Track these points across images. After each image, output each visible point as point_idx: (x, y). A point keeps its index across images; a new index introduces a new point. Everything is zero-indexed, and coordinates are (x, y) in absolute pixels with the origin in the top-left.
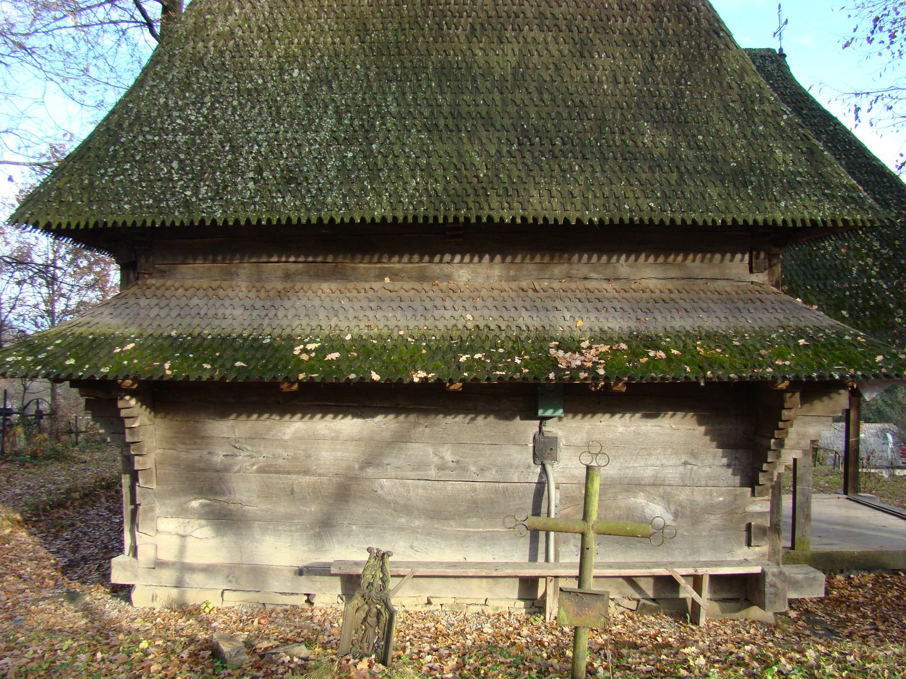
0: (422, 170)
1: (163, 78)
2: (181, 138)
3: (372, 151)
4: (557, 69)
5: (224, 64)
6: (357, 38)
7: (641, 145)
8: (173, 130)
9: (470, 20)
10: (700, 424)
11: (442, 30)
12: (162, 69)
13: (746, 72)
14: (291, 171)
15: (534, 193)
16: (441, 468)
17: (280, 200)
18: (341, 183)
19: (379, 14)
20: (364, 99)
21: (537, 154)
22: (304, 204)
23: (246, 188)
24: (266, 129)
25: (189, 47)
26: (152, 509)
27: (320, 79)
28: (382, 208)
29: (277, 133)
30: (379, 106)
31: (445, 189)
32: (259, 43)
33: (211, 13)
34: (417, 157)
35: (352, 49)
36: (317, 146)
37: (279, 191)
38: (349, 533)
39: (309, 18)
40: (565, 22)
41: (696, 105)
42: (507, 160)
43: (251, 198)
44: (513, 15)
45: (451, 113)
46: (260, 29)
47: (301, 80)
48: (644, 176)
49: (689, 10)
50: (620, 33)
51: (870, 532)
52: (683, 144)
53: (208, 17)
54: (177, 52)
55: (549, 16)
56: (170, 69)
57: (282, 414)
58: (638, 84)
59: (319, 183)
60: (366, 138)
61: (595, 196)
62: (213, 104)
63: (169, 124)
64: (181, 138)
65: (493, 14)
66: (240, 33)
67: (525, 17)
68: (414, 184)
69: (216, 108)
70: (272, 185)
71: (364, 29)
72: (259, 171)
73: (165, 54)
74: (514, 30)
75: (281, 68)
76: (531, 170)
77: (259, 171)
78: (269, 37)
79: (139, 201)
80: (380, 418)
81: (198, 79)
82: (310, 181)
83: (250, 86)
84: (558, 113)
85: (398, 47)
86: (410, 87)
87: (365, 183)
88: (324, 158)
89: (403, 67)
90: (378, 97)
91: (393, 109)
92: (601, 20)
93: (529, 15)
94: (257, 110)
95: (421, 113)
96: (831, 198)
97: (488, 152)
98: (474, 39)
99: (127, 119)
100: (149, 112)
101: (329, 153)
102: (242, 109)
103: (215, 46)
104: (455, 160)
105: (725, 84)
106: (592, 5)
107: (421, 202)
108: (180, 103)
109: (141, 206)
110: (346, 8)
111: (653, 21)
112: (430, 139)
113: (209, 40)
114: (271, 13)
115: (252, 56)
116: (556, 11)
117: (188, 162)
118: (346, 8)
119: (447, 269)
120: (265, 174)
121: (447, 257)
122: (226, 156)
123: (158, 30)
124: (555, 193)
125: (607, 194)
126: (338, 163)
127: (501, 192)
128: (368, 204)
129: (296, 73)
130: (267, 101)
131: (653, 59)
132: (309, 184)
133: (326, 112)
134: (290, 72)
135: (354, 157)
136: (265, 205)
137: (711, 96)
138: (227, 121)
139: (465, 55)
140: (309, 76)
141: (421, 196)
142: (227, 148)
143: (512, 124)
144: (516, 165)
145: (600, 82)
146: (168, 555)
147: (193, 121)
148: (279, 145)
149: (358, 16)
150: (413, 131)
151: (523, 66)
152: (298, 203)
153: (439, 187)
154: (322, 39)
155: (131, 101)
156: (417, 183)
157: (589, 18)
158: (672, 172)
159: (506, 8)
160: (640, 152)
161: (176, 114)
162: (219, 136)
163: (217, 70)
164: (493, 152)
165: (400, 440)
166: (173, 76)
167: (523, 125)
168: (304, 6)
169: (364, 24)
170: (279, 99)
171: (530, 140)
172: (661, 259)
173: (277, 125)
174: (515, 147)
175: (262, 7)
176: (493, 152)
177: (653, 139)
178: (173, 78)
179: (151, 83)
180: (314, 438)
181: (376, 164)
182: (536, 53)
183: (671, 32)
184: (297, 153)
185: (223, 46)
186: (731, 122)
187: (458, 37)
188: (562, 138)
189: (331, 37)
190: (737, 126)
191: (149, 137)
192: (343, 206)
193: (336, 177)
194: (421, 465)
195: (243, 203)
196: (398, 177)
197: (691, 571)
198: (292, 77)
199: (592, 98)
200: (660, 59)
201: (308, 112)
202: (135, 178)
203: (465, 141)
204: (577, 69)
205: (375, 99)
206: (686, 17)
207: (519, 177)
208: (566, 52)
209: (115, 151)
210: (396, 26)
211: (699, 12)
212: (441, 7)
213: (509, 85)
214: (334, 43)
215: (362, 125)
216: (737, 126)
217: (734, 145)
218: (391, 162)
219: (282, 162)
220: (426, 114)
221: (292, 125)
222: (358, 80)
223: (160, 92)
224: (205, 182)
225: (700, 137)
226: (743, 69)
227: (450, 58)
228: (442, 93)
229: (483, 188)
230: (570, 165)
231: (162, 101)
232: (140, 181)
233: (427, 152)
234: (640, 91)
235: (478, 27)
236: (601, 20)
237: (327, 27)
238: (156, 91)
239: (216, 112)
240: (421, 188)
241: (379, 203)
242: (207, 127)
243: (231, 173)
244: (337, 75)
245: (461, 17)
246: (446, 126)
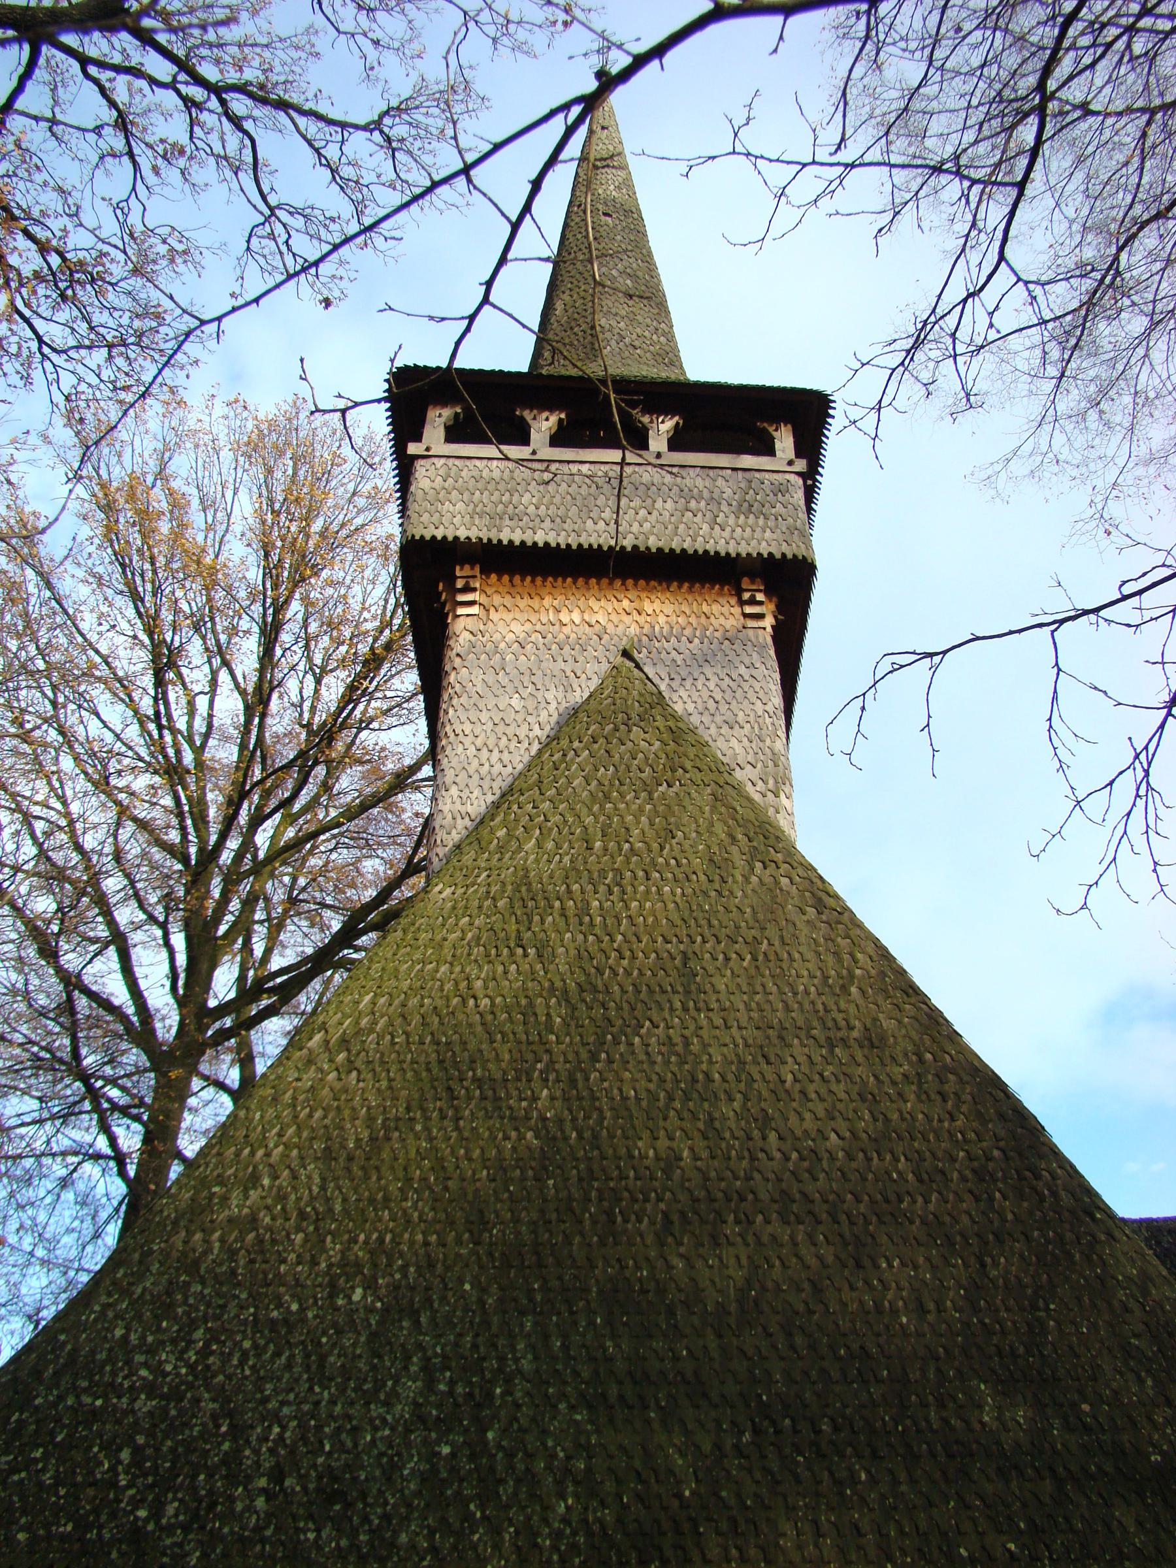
0: (576, 1483)
1: (125, 1292)
2: (145, 1405)
3: (485, 1442)
4: (817, 1289)
5: (233, 1273)
6: (467, 1235)
7: (977, 1427)
8: (132, 1387)
9: (662, 1206)
11: (614, 1222)
12: (126, 1275)
13: (1152, 1280)
14: (336, 1479)
15: (787, 1527)
17: (311, 1536)
18: (427, 1505)
19: (506, 1195)
20: (475, 1346)
21: (787, 1451)
22: (354, 1546)
23: (250, 1509)
24: (297, 1396)
25: (178, 1240)
28: (501, 1557)
29: (317, 1404)
30: (502, 1359)
31: (619, 1520)
32: (299, 1238)
33: (222, 1184)
34: (569, 1458)
35: (458, 1255)
36: (387, 1432)
37: (311, 1517)
39: (386, 1199)
40: (825, 1207)
41: (1071, 1348)
42: (734, 1464)
43: (258, 1529)
44: (735, 1196)
45: (630, 1373)
46: (302, 1215)
47: (365, 1307)
48: (989, 1488)
49: (1038, 1177)
50: (922, 1222)
52: (1057, 1422)
53: (216, 1189)
54: (156, 1247)
55: (798, 1196)
56: (141, 1277)
58: (960, 1311)
59: (386, 1503)
60: (476, 1419)
61: (901, 1532)
62: (207, 1345)
63: (125, 1378)
64: (145, 1405)
65: (700, 1194)
66: (267, 1220)
67: (756, 1199)
68: (562, 1508)
69: (213, 1352)
70: (300, 1504)
71: (478, 1223)
72: (277, 1475)
73: (134, 1250)
74: (737, 1222)
75: (333, 1285)
76: (778, 1483)
77: (277, 1475)
78: (317, 1229)
79: (47, 1526)
81: (186, 1298)
82: (370, 1500)
83: (275, 1314)
84: (823, 1371)
85: (537, 1253)
86: (557, 1324)
87: (472, 1507)
88: (399, 1454)
89: (545, 1288)
90: (501, 1342)
91: (526, 1364)
92: (887, 1201)
93: (763, 1195)
94: (283, 1359)
95: (576, 1373)
97: (698, 1447)
98: (670, 1240)
99: (51, 1362)
100: (93, 1352)
101: (408, 1445)
102: (258, 1356)
103: (222, 1240)
104: (637, 1464)
105: (1116, 1303)
106: (870, 1176)
107: (574, 1546)
108: (150, 1339)
109: (49, 1537)
110: (450, 1183)
111: (977, 1199)
112: (592, 1422)
113: (214, 1231)
114: (323, 1188)
115: (284, 1261)
116: (810, 1188)
117: (149, 1451)
118: (450, 1183)
120: (288, 1482)
122: (220, 1444)
123: (132, 1170)
124: (825, 1527)
125: (923, 1526)
126: (424, 1466)
127: (724, 1526)
128: (474, 1547)
129: (358, 1294)
130: (303, 1342)
131: (983, 1265)
132: (366, 1505)
133: (406, 1368)
134: (348, 1292)
135: (453, 1455)
136: (283, 1544)
137: (1093, 1327)
138: (229, 1377)
139: (653, 1268)
140: (381, 1300)
141: (574, 1533)
142: (224, 1429)
143: (741, 1394)
144: (750, 1472)
145: (895, 1312)
147: (169, 1373)
148: (319, 1428)
149: (470, 1197)
150: (562, 1406)
151: (757, 1286)
152: (344, 1543)
153: (608, 1515)
154: (406, 1236)
155: (63, 1331)
156: (568, 1508)
157: (866, 1198)
158: (1043, 1479)
159: (723, 1184)
160: (977, 1442)
161: (139, 1358)
162: (211, 1405)
163: (221, 1284)
164: (707, 1447)
166: (145, 1289)
167: (760, 1396)
168: (379, 1179)
169: (481, 1212)
170: (324, 1340)
171: (774, 1423)
173: (317, 1389)
174: (747, 1437)
175: (309, 1177)
176: (707, 1447)
178: (143, 1293)
179: (104, 1299)
181: (492, 1469)
182: (777, 1263)
183: (1010, 1217)
184: (349, 1444)
185: (236, 1241)
186: (1139, 1377)
187: (642, 1236)
188: (832, 1420)
189: (423, 1233)
190: (1149, 1382)
191: (87, 1400)
192: (427, 1551)
193: (418, 1494)
195: (242, 1540)
196: (532, 1496)
198: (350, 1301)
199: (881, 1340)
200: (996, 1264)
201: (374, 1368)
202: (47, 1478)
203: (656, 1426)
204: (852, 1288)
205: (495, 1346)
206: (1033, 1188)
207: (756, 1495)
208: (830, 1259)
209: (18, 1421)
210: (535, 1215)
211: (1054, 1178)
212: (612, 1184)
213: (732, 1321)
214: (426, 1244)
215: (471, 1395)
216: (1149, 1382)
217: (1150, 1419)
218: (521, 1467)
219: (321, 1460)
220: (585, 1375)
221: (344, 1391)
222: (466, 1309)
223: (116, 1317)
224: (175, 1493)
225: (1086, 1407)
226: (1145, 1276)
227: (627, 1273)
228: (613, 1337)
229: (690, 1519)
230: (850, 1469)
231: (119, 1332)
232: (56, 1485)
233: (587, 1447)
234: (967, 1324)
235: (675, 1217)
236: (887, 1201)
237: (416, 1214)
238: (111, 1314)
239: (211, 1360)
240: (575, 1518)
241: (497, 1547)
242: (191, 1386)
243: (226, 1477)
244: (429, 1300)
245: (646, 1200)
246: (621, 1397)
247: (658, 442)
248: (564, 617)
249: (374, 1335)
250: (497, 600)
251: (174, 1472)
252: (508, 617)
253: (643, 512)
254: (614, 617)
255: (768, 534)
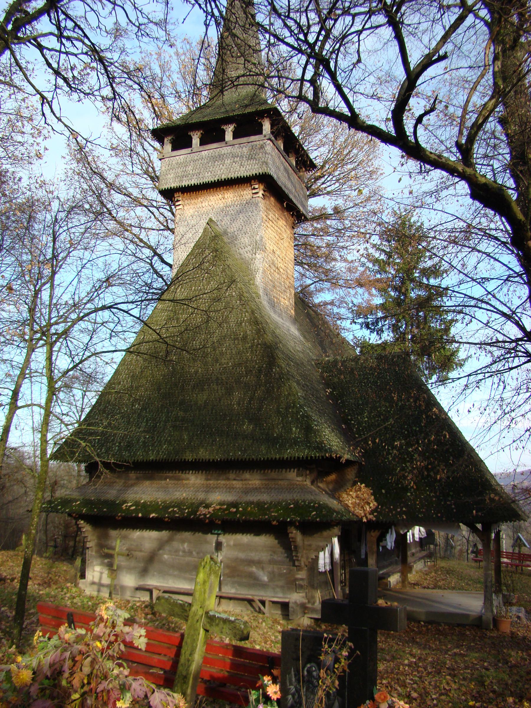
10: (276, 539)
16: (184, 551)
26: (92, 562)
27: (144, 408)
38: (153, 575)
51: (420, 600)
57: (133, 529)
72: (120, 443)
77: (120, 443)
80: (164, 532)
96: (309, 448)
119: (187, 476)
121: (187, 472)
146: (96, 580)
165: (170, 540)
172: (262, 472)
177: (247, 427)
180: (143, 538)
194: (177, 551)
197: (261, 598)
247: (229, 136)
248: (203, 205)
249: (139, 414)
250: (186, 201)
251: (104, 443)
252: (189, 207)
253: (221, 166)
254: (217, 202)
255: (256, 166)
